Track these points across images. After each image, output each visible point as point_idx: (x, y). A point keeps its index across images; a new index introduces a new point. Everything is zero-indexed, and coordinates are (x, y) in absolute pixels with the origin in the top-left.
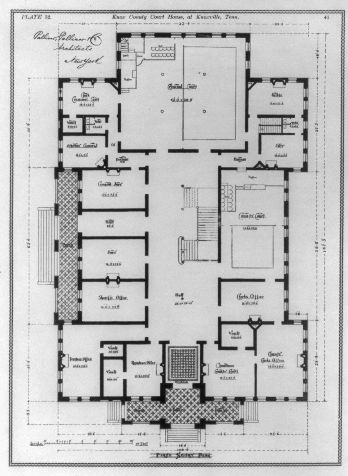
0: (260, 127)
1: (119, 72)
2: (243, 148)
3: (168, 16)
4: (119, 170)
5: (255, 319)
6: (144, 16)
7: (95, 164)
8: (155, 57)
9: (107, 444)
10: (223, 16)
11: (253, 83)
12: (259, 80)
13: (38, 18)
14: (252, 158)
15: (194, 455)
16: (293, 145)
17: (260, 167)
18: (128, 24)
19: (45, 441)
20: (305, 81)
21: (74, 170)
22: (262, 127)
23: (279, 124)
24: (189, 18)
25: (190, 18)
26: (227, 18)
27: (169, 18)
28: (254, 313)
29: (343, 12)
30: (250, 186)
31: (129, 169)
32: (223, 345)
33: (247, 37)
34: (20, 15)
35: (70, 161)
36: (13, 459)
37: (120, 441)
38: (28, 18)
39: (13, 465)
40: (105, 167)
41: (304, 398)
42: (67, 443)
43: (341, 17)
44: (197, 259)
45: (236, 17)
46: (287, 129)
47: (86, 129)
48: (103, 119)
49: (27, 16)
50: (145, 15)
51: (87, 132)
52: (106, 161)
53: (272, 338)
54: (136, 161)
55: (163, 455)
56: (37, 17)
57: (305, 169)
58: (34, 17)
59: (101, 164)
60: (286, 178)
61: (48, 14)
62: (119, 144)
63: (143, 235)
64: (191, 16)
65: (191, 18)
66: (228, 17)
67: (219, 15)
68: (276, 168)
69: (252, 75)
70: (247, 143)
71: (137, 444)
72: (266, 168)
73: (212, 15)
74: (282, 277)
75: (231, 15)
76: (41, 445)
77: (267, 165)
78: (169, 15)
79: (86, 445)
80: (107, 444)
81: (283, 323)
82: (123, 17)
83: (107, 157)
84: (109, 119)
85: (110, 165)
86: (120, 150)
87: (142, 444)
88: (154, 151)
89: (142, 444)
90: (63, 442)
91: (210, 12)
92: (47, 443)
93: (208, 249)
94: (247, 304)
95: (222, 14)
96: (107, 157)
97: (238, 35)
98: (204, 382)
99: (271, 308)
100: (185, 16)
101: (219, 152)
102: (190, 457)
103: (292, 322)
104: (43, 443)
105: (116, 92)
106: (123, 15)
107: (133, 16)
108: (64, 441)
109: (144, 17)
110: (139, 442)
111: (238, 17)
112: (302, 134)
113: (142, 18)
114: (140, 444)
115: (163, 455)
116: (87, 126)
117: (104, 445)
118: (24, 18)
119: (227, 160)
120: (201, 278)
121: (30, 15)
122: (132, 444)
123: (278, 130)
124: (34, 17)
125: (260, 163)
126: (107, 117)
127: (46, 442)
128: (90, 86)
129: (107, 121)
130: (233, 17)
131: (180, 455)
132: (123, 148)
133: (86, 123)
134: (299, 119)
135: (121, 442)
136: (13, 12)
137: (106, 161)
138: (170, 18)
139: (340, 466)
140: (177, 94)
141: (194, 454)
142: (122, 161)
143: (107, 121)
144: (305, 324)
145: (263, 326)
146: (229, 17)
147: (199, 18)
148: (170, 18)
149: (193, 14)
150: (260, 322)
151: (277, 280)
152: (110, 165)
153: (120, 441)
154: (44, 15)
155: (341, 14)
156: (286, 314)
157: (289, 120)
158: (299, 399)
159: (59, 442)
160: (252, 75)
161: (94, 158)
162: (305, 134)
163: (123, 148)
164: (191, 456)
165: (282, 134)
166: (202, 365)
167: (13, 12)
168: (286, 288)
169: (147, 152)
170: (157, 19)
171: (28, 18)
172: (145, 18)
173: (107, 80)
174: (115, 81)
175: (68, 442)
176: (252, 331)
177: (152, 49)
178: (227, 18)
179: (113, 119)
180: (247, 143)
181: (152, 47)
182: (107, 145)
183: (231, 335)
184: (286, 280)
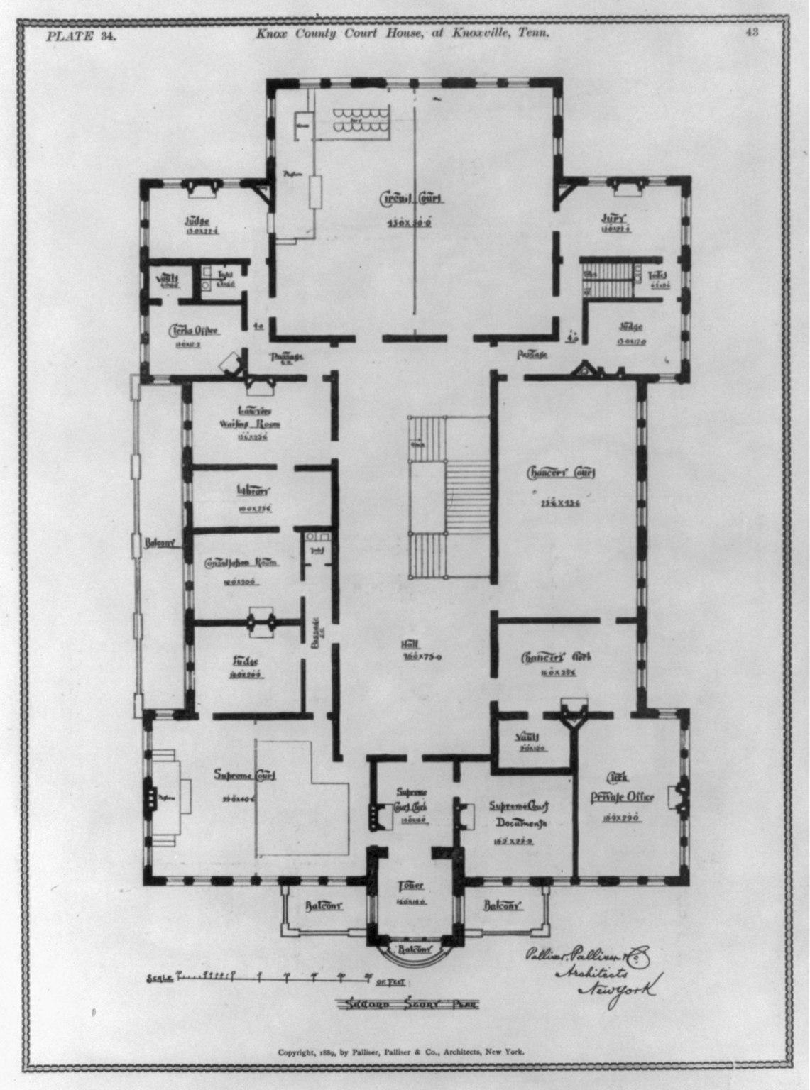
0: (585, 283)
1: (271, 163)
2: (548, 331)
3: (388, 31)
4: (272, 380)
5: (574, 707)
6: (330, 31)
7: (219, 366)
8: (343, 132)
9: (259, 980)
10: (513, 29)
11: (569, 186)
12: (583, 181)
13: (86, 39)
14: (562, 357)
15: (439, 1005)
16: (661, 321)
17: (588, 373)
18: (289, 55)
19: (179, 973)
20: (684, 184)
21: (175, 379)
22: (589, 283)
23: (626, 277)
24: (437, 35)
25: (438, 34)
26: (522, 35)
27: (388, 36)
28: (573, 694)
29: (786, 19)
30: (442, 457)
31: (302, 378)
32: (503, 764)
33: (556, 85)
34: (44, 32)
35: (167, 359)
36: (31, 1057)
37: (341, 975)
38: (63, 40)
39: (32, 1069)
40: (241, 374)
41: (682, 879)
42: (227, 979)
43: (781, 30)
44: (446, 575)
45: (543, 33)
46: (643, 290)
47: (202, 289)
48: (237, 269)
49: (59, 33)
50: (332, 28)
51: (205, 296)
52: (244, 358)
53: (614, 747)
54: (317, 360)
55: (428, 1004)
56: (82, 37)
57: (684, 377)
58: (75, 37)
59: (233, 366)
60: (642, 396)
61: (108, 30)
62: (273, 322)
63: (298, 535)
64: (442, 30)
65: (440, 35)
66: (525, 32)
67: (506, 27)
68: (622, 375)
69: (568, 171)
70: (556, 321)
71: (380, 983)
72: (598, 375)
73: (491, 27)
74: (633, 613)
75: (531, 27)
76: (170, 979)
77: (601, 369)
78: (390, 29)
79: (323, 983)
80: (287, 980)
81: (634, 715)
82: (478, 33)
83: (245, 351)
84: (250, 268)
85: (253, 369)
86: (274, 338)
87: (392, 983)
88: (351, 339)
89: (392, 983)
90: (219, 977)
91: (379, 20)
92: (184, 978)
93: (470, 552)
94: (551, 673)
95: (522, 15)
96: (245, 351)
97: (536, 83)
98: (463, 844)
99: (607, 685)
100: (426, 30)
101: (494, 340)
102: (432, 1008)
103: (654, 714)
104: (175, 977)
105: (266, 207)
106: (415, 28)
107: (304, 31)
108: (219, 975)
109: (329, 34)
110: (386, 977)
111: (546, 33)
112: (679, 300)
113: (326, 36)
114: (387, 983)
115: (428, 1004)
116: (205, 285)
117: (254, 982)
118: (53, 39)
119: (505, 358)
120: (452, 617)
121: (66, 32)
122: (368, 981)
123: (624, 290)
124: (75, 37)
125: (585, 363)
126: (244, 263)
127: (181, 976)
128: (208, 196)
129: (245, 273)
130: (535, 34)
131: (353, 1004)
132: (280, 331)
133: (203, 277)
134: (671, 267)
135: (316, 978)
136: (22, 24)
137: (244, 358)
138: (392, 35)
139: (792, 1067)
140: (403, 212)
141: (439, 1001)
142: (285, 361)
143: (245, 273)
144: (684, 716)
145: (591, 723)
146: (528, 33)
147: (459, 36)
148: (392, 35)
149: (445, 27)
150: (586, 715)
151: (620, 621)
152: (253, 369)
153: (341, 975)
154: (98, 32)
155: (781, 24)
156: (642, 694)
157: (647, 268)
158: (670, 881)
159: (208, 976)
160: (568, 171)
161: (215, 355)
162: (685, 301)
163: (280, 331)
164: (433, 1005)
165: (634, 299)
166: (458, 808)
167: (22, 24)
168: (642, 637)
169: (334, 341)
170: (360, 38)
171: (63, 40)
172: (333, 35)
173: (246, 183)
174: (264, 185)
175: (230, 977)
176: (567, 732)
177: (334, 114)
178: (522, 35)
179: (259, 269)
180: (556, 321)
181: (334, 110)
182: (245, 326)
183: (541, 743)
184: (641, 620)
